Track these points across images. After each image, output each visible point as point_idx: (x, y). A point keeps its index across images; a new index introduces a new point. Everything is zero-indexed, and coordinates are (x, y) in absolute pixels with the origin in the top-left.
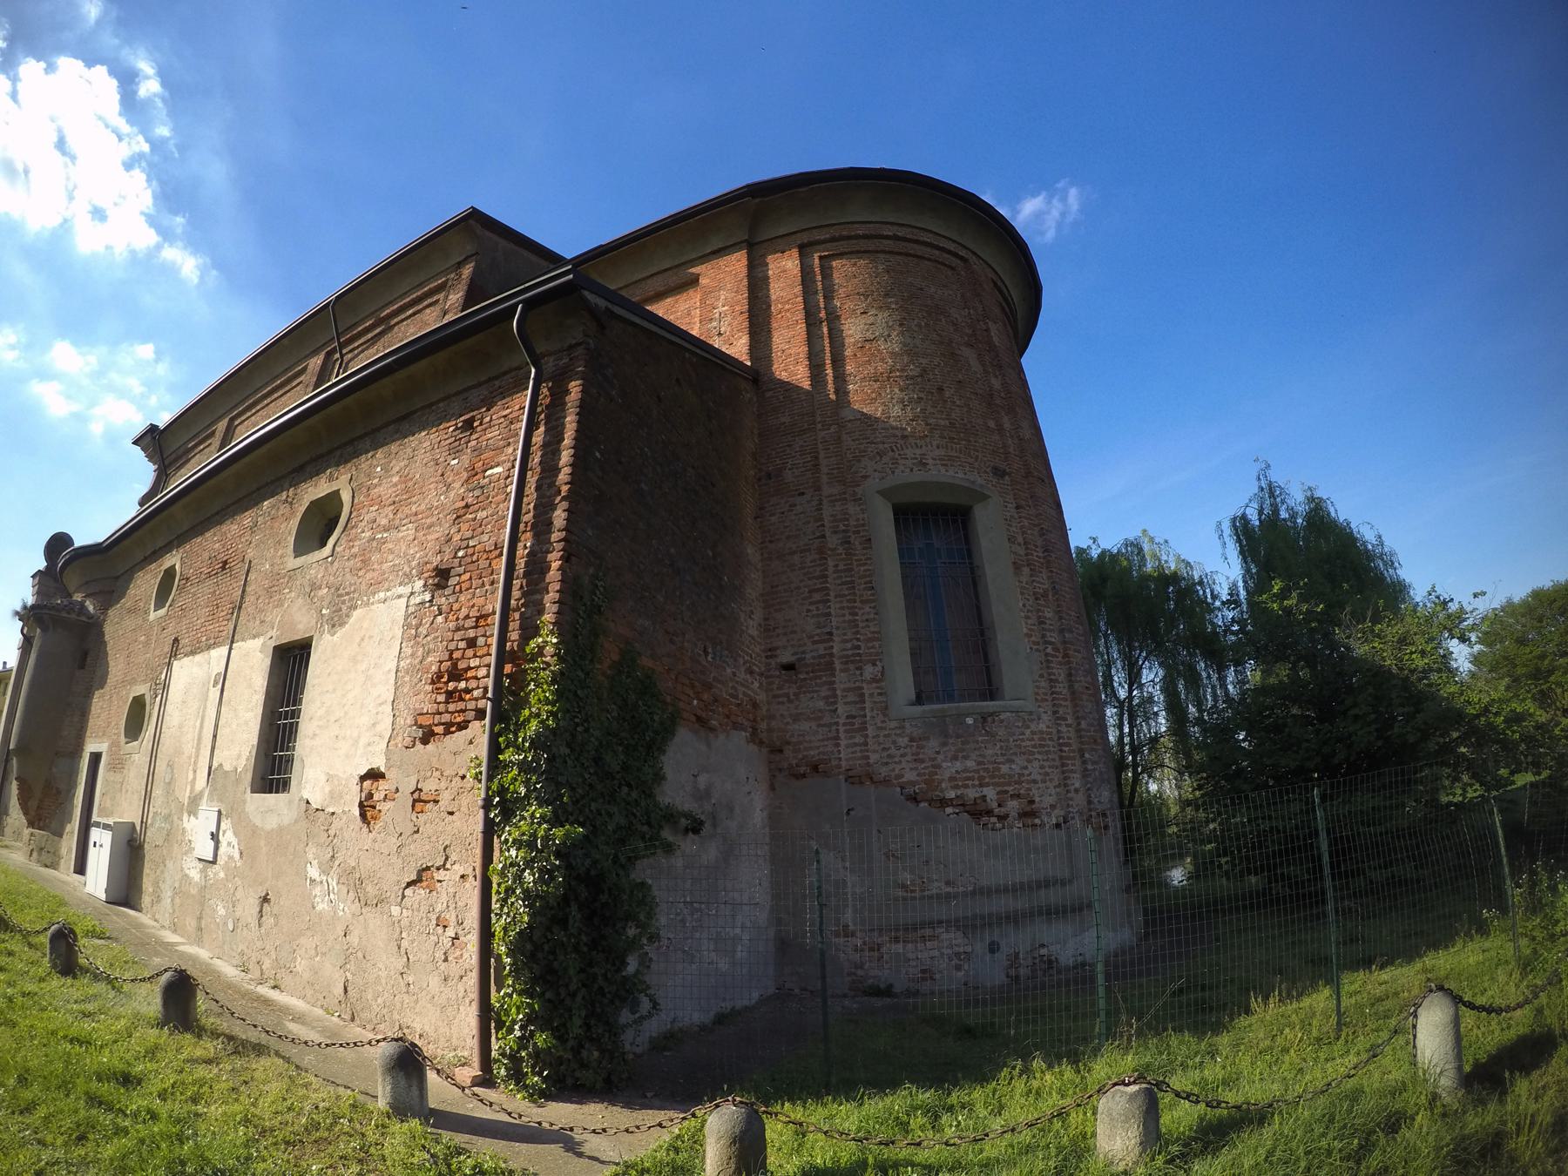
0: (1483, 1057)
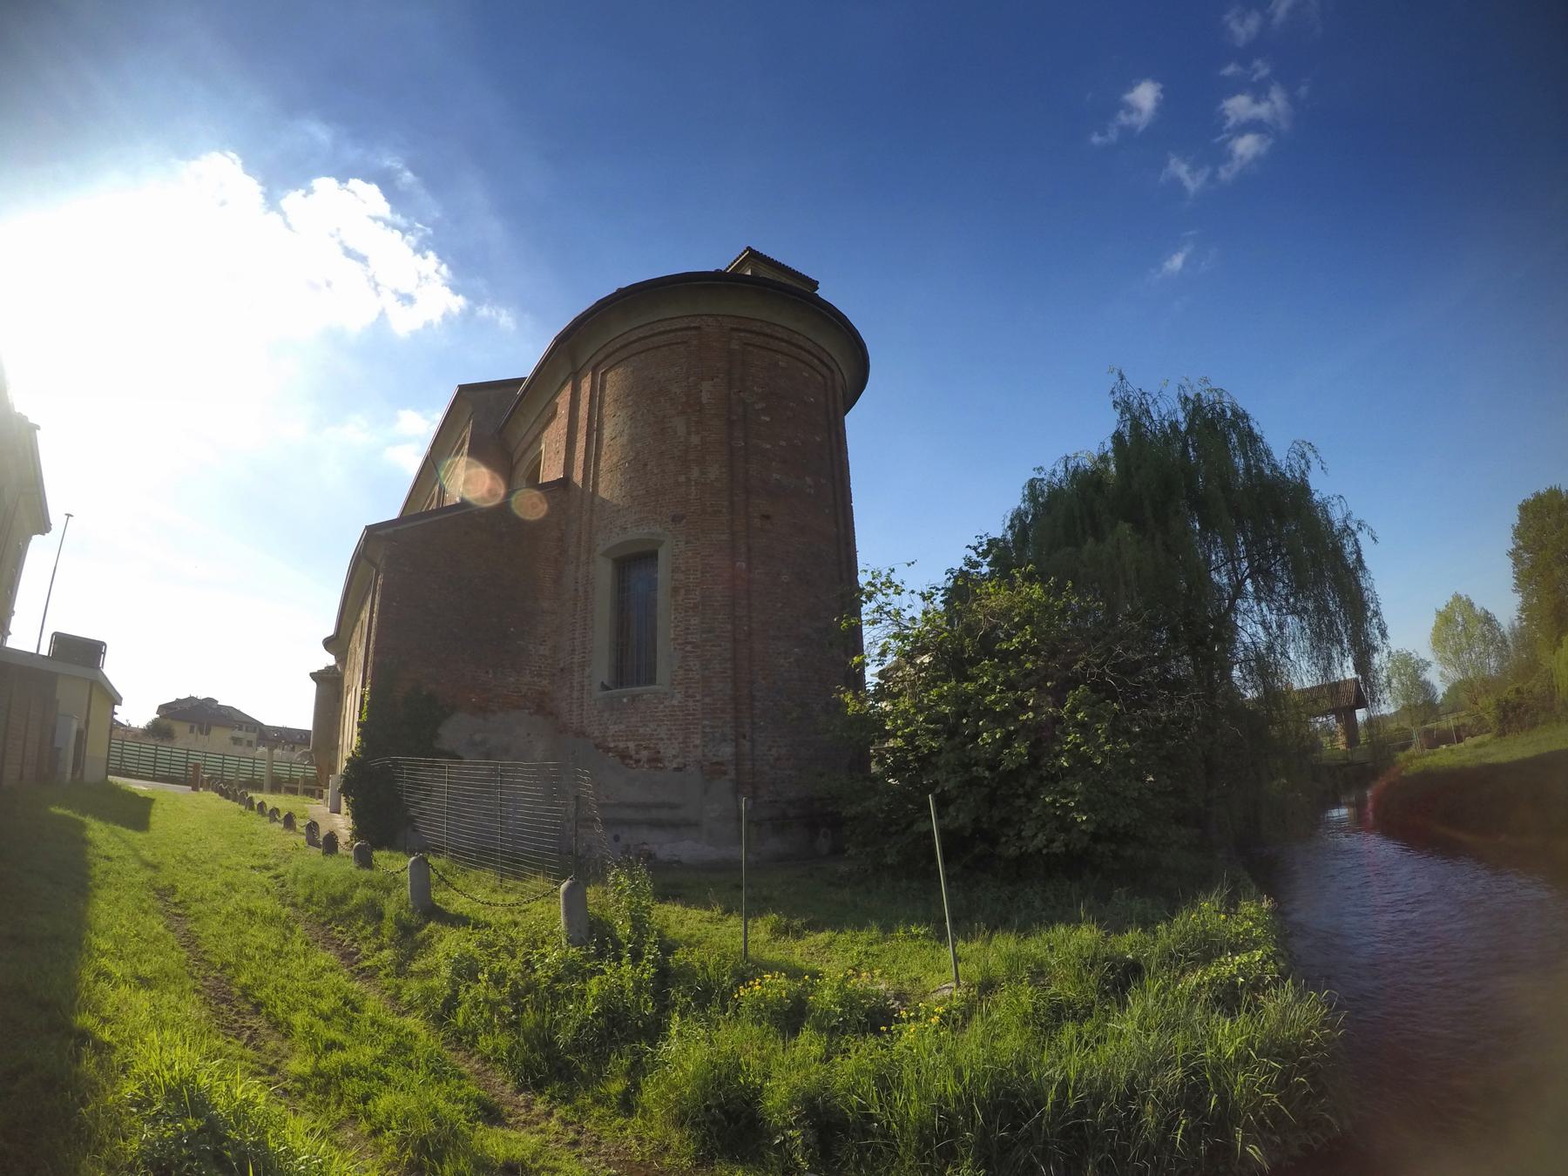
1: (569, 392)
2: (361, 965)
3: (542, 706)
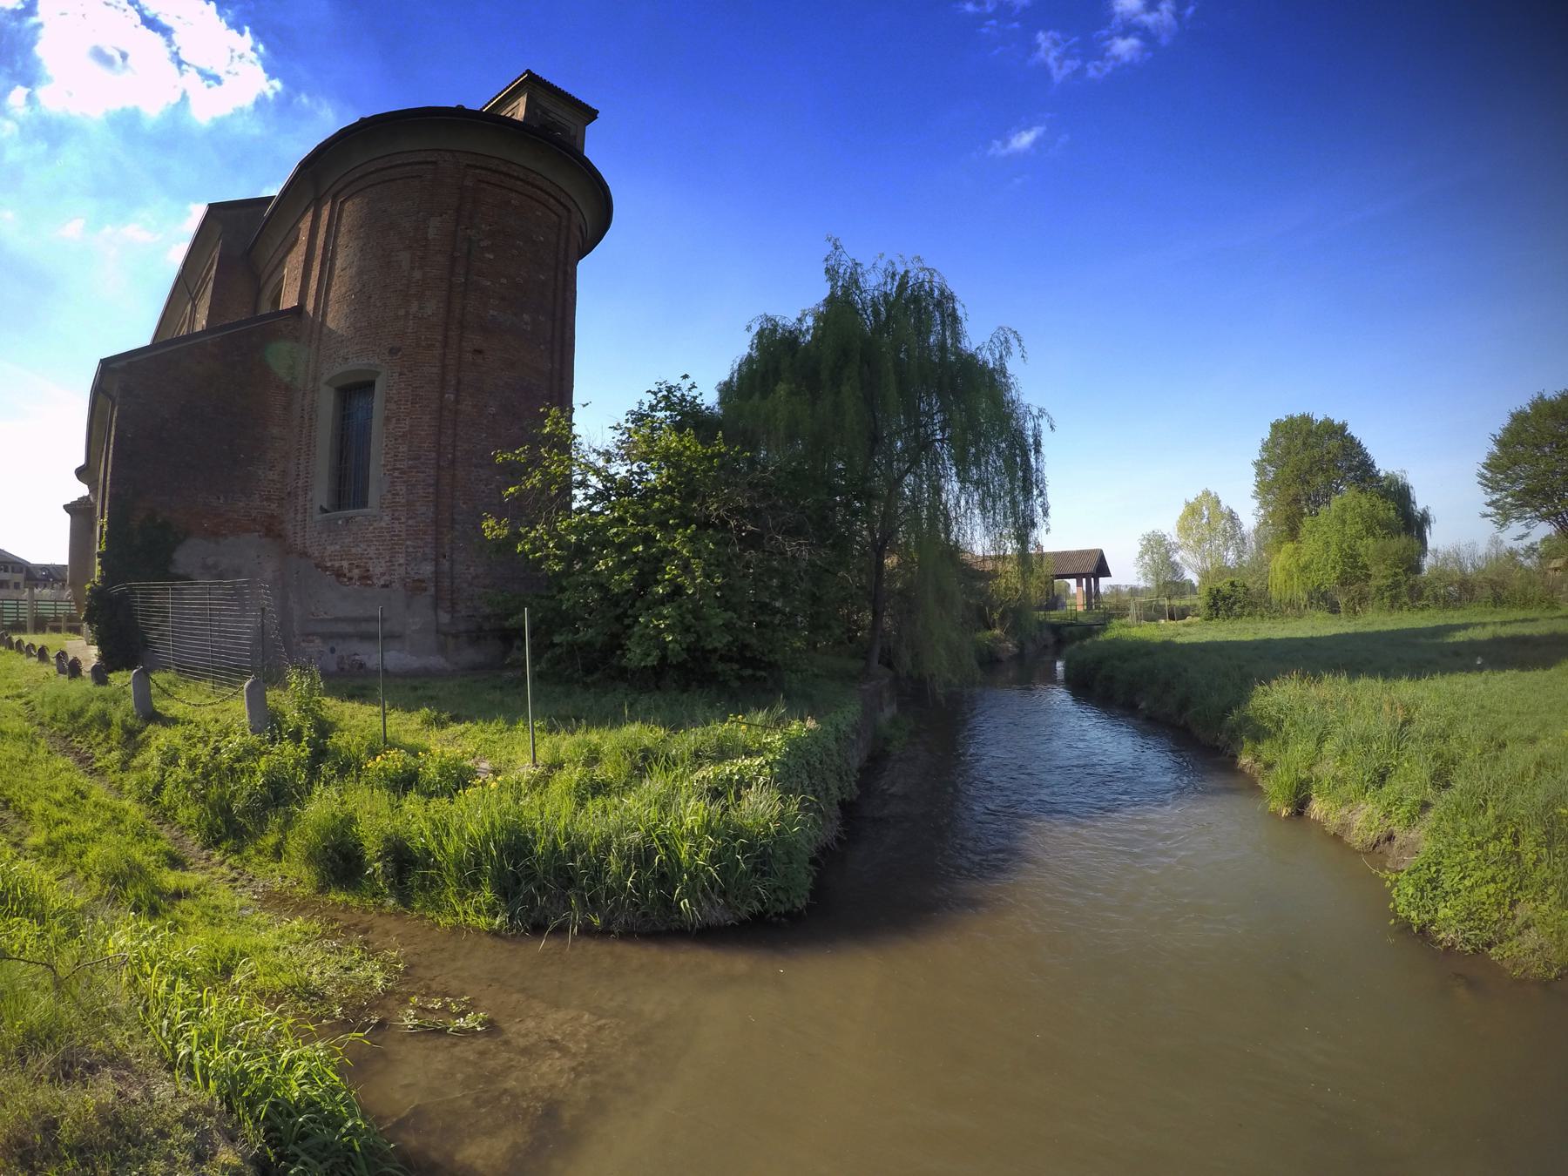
0: (124, 673)
1: (310, 219)
2: (94, 766)
3: (272, 530)
